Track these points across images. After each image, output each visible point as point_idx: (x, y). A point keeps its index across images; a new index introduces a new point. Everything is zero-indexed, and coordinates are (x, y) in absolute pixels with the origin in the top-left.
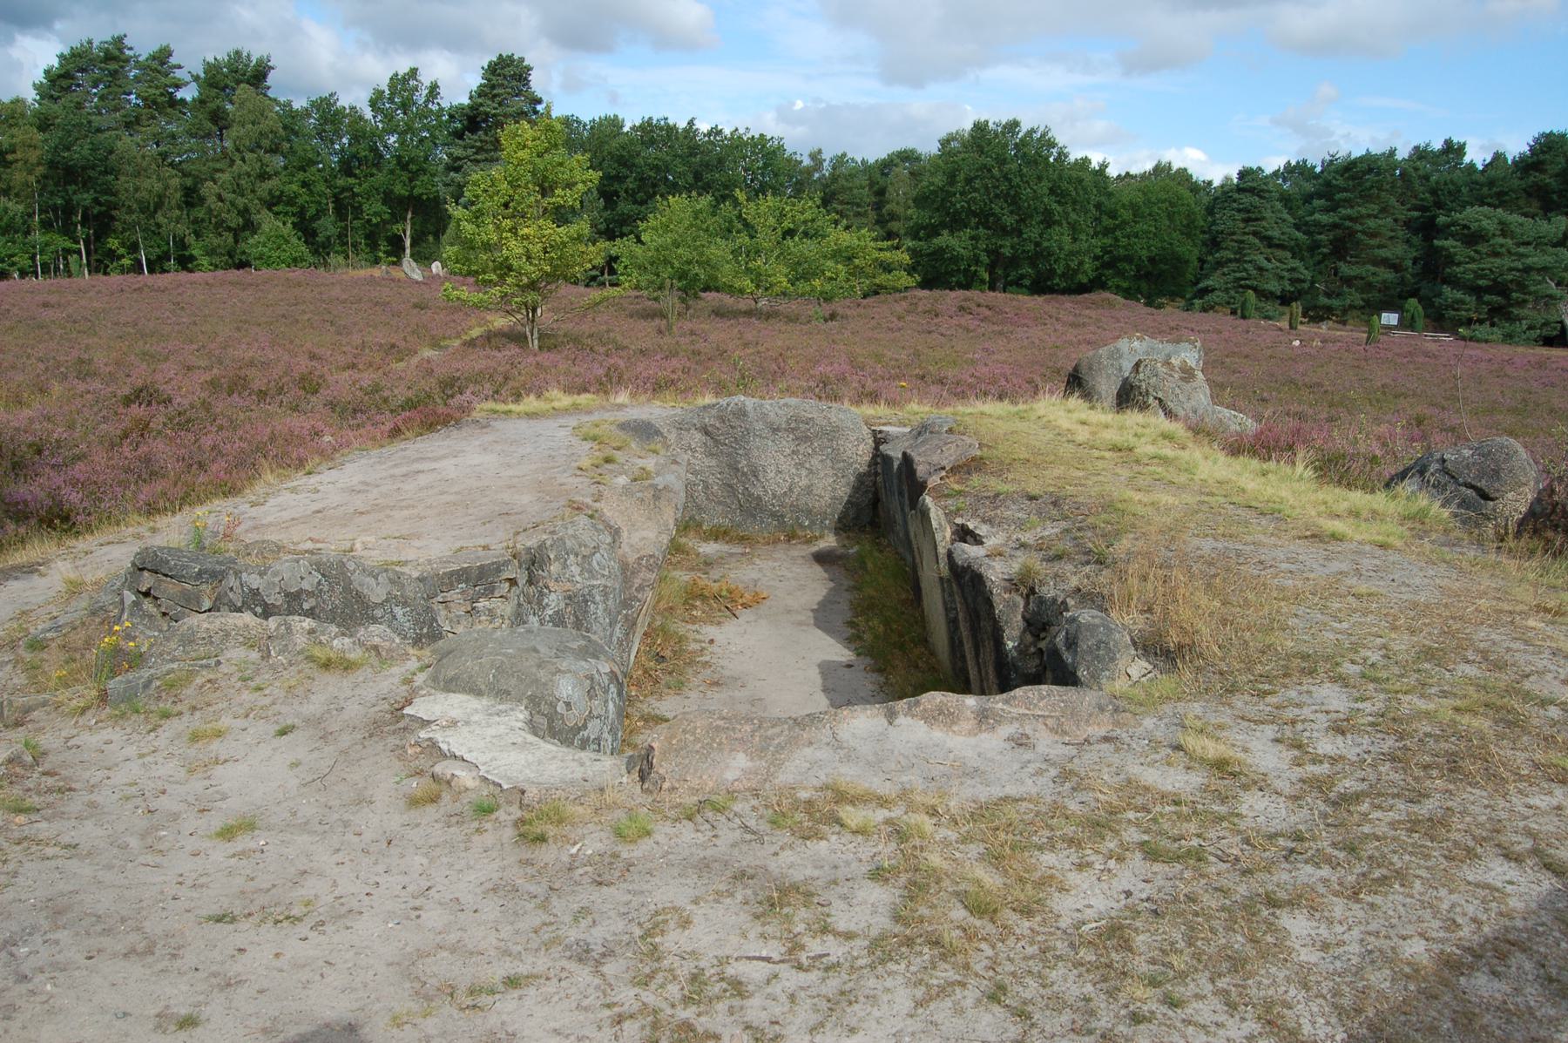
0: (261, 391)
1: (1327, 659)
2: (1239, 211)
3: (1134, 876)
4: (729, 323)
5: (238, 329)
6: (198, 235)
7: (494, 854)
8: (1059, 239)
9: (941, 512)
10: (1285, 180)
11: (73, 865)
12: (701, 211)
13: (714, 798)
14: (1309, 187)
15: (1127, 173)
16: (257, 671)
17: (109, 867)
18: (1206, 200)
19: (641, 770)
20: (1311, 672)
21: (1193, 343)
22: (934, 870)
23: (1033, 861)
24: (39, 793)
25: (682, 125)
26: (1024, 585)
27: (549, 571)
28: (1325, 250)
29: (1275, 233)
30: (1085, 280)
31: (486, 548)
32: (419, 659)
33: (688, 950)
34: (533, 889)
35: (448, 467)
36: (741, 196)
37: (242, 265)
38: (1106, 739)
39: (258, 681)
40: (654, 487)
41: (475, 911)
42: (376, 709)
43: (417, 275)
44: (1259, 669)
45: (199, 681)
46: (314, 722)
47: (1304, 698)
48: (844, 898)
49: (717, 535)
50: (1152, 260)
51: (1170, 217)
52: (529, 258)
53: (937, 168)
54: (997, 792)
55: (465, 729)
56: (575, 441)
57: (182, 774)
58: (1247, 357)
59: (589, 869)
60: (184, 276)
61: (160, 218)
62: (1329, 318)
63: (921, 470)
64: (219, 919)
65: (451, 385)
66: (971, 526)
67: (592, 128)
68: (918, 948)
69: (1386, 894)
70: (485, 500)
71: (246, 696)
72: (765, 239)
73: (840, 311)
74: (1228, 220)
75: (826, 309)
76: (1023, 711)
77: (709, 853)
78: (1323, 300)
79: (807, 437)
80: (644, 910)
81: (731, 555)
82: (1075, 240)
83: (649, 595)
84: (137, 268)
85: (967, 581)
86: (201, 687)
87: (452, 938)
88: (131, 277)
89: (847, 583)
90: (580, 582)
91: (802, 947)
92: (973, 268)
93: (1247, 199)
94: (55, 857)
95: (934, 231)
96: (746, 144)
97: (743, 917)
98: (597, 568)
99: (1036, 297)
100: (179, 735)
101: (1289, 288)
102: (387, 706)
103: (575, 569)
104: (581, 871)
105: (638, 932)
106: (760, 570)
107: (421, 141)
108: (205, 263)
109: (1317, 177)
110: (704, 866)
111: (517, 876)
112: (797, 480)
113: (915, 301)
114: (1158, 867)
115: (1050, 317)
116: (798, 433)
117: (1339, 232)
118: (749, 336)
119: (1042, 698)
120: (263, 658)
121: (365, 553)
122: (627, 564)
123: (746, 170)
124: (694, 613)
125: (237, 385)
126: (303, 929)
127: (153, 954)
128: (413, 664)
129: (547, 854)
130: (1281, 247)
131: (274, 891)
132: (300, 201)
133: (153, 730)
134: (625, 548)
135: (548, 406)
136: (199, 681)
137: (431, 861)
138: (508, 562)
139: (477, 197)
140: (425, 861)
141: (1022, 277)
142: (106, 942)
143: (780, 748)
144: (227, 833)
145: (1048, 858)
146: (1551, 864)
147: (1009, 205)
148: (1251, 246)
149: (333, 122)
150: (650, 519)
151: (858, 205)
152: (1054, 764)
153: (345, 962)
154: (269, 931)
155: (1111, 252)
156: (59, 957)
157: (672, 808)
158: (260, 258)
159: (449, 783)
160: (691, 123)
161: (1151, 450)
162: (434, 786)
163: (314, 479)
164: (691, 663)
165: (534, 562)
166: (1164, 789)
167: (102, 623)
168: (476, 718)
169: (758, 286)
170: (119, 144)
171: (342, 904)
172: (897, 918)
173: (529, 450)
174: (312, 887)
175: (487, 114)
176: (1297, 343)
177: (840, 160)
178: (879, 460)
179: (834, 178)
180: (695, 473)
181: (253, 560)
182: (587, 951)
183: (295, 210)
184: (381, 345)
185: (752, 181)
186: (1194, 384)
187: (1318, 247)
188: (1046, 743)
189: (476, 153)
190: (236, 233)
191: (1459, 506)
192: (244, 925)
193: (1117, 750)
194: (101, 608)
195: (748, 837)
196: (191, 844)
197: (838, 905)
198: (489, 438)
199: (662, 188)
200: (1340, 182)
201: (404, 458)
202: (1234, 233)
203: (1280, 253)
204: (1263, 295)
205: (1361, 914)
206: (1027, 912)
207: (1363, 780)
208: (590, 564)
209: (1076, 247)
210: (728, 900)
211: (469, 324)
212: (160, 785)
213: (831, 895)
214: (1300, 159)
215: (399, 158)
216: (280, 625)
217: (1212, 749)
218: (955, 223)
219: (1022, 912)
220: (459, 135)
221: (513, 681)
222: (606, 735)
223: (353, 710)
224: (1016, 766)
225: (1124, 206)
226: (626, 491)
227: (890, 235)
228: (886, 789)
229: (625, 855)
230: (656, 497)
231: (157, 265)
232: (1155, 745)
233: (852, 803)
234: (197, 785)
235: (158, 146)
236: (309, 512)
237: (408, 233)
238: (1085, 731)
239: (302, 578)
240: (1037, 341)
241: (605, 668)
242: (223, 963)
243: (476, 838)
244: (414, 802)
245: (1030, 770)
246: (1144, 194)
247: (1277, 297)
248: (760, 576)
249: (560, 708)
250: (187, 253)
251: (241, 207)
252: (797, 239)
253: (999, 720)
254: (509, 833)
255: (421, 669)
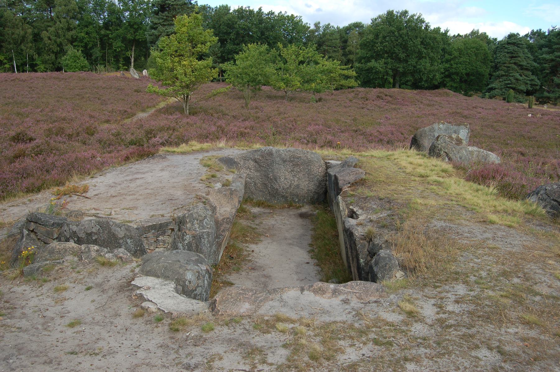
0: (69, 134)
1: (464, 274)
2: (508, 53)
3: (367, 350)
4: (274, 102)
5: (58, 101)
6: (39, 54)
7: (161, 334)
8: (425, 64)
9: (344, 203)
10: (531, 38)
11: (21, 334)
12: (262, 52)
13: (235, 318)
14: (542, 42)
15: (459, 34)
16: (78, 266)
17: (34, 335)
18: (494, 47)
19: (212, 308)
20: (457, 279)
21: (466, 126)
22: (303, 344)
23: (336, 343)
24: (5, 309)
25: (256, 10)
26: (369, 238)
27: (186, 227)
28: (547, 71)
29: (524, 63)
30: (436, 83)
31: (163, 216)
32: (137, 262)
33: (221, 367)
34: (173, 346)
35: (149, 177)
36: (280, 45)
37: (59, 69)
38: (376, 302)
39: (78, 269)
40: (230, 189)
41: (155, 353)
42: (121, 281)
43: (136, 76)
44: (438, 278)
45: (56, 268)
46: (99, 285)
47: (451, 289)
48: (273, 352)
49: (259, 204)
50: (467, 74)
51: (476, 55)
52: (186, 75)
53: (371, 31)
54: (332, 319)
55: (153, 290)
56: (201, 167)
57: (53, 303)
58: (504, 122)
59: (192, 340)
60: (33, 74)
61: (23, 47)
62: (548, 102)
63: (341, 183)
64: (72, 353)
65: (150, 134)
66: (355, 210)
67: (216, 10)
68: (291, 369)
69: (442, 358)
70: (163, 193)
71: (74, 274)
72: (292, 66)
73: (323, 97)
74: (502, 57)
75: (318, 96)
76: (350, 290)
77: (232, 336)
78: (546, 94)
79: (298, 165)
80: (209, 354)
81: (265, 213)
82: (432, 65)
83: (227, 234)
84: (12, 69)
85: (349, 233)
86: (58, 271)
87: (147, 361)
88: (9, 75)
89: (311, 227)
90: (198, 230)
91: (256, 367)
92: (385, 77)
93: (511, 48)
94: (15, 331)
95: (368, 60)
96: (285, 19)
97: (239, 357)
98: (205, 225)
99: (414, 90)
100: (50, 289)
101: (530, 88)
102: (125, 280)
103: (197, 226)
104: (189, 341)
105: (206, 361)
106: (276, 220)
107: (140, 15)
108: (42, 67)
109: (545, 37)
110: (230, 341)
111: (169, 342)
112: (293, 182)
113: (357, 93)
114: (376, 347)
115: (418, 101)
116: (294, 163)
117: (553, 63)
118: (282, 110)
119: (357, 285)
120: (79, 260)
121: (116, 216)
122: (218, 221)
123: (284, 30)
124: (247, 239)
125: (60, 132)
126: (99, 357)
127: (52, 363)
128: (134, 264)
129: (179, 335)
130: (527, 69)
131: (88, 345)
132: (85, 41)
133: (41, 286)
134: (218, 215)
135: (190, 149)
136: (56, 268)
137: (141, 336)
138: (170, 222)
139: (164, 47)
140: (138, 336)
141: (408, 81)
142: (37, 359)
143: (261, 301)
144: (72, 325)
145: (342, 343)
146: (500, 351)
147: (403, 49)
148: (513, 69)
149: (100, 6)
150: (228, 203)
151: (335, 47)
152: (355, 310)
153: (113, 367)
154: (88, 357)
155: (449, 70)
156: (22, 363)
157: (221, 321)
158: (67, 66)
159: (147, 310)
160: (260, 9)
161: (435, 178)
162: (142, 311)
163: (94, 180)
164: (244, 260)
165: (181, 222)
166: (388, 320)
167: (13, 240)
168: (156, 286)
169: (287, 86)
170: (5, 13)
171: (111, 350)
172: (289, 360)
173: (182, 170)
174: (101, 344)
175: (169, 4)
176: (530, 115)
177: (327, 27)
178: (327, 174)
179: (324, 34)
180: (250, 178)
181: (73, 219)
182: (190, 366)
183: (83, 44)
184: (120, 111)
185: (287, 35)
186: (461, 147)
187: (544, 70)
188: (355, 303)
189: (163, 22)
190: (56, 54)
191: (551, 208)
192: (80, 355)
193: (378, 306)
194: (13, 234)
195: (245, 332)
196: (60, 328)
197: (270, 355)
198: (165, 164)
199: (246, 38)
200: (555, 40)
201: (131, 172)
202: (505, 63)
203: (526, 72)
204: (520, 92)
205: (431, 364)
206: (328, 359)
207: (456, 320)
208: (203, 223)
209: (432, 68)
210: (235, 352)
211: (159, 100)
212: (46, 307)
213: (268, 352)
214: (538, 29)
215: (129, 22)
216: (86, 248)
217: (408, 307)
218: (378, 56)
219: (327, 359)
220: (156, 13)
221: (171, 273)
222: (204, 293)
223: (113, 281)
224: (342, 310)
225: (455, 50)
226: (219, 191)
227: (348, 62)
228: (294, 316)
229: (204, 336)
230: (231, 194)
231: (21, 68)
232: (391, 304)
233: (282, 321)
234: (59, 308)
235: (22, 14)
236: (92, 195)
237: (133, 56)
238: (369, 298)
239: (92, 228)
240: (410, 114)
241: (204, 267)
242: (75, 367)
243: (155, 329)
244: (136, 316)
245: (346, 312)
246: (465, 44)
247: (524, 93)
248: (275, 223)
249: (187, 283)
250: (34, 63)
251: (58, 43)
252: (304, 65)
253: (340, 293)
254: (166, 328)
255: (138, 266)
